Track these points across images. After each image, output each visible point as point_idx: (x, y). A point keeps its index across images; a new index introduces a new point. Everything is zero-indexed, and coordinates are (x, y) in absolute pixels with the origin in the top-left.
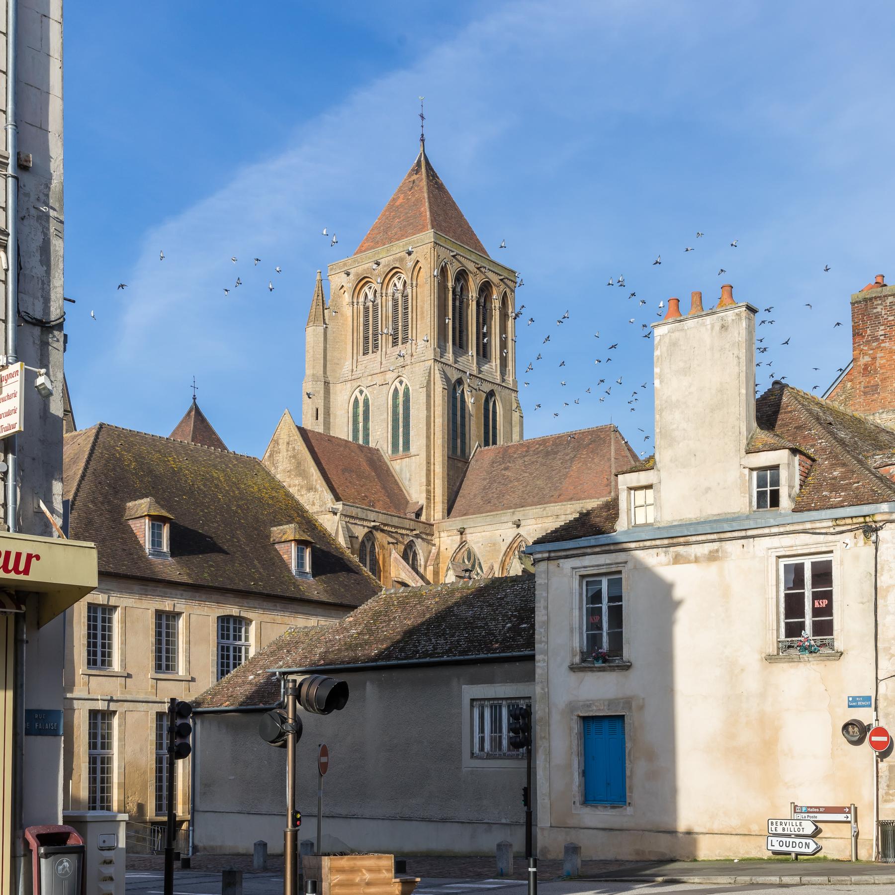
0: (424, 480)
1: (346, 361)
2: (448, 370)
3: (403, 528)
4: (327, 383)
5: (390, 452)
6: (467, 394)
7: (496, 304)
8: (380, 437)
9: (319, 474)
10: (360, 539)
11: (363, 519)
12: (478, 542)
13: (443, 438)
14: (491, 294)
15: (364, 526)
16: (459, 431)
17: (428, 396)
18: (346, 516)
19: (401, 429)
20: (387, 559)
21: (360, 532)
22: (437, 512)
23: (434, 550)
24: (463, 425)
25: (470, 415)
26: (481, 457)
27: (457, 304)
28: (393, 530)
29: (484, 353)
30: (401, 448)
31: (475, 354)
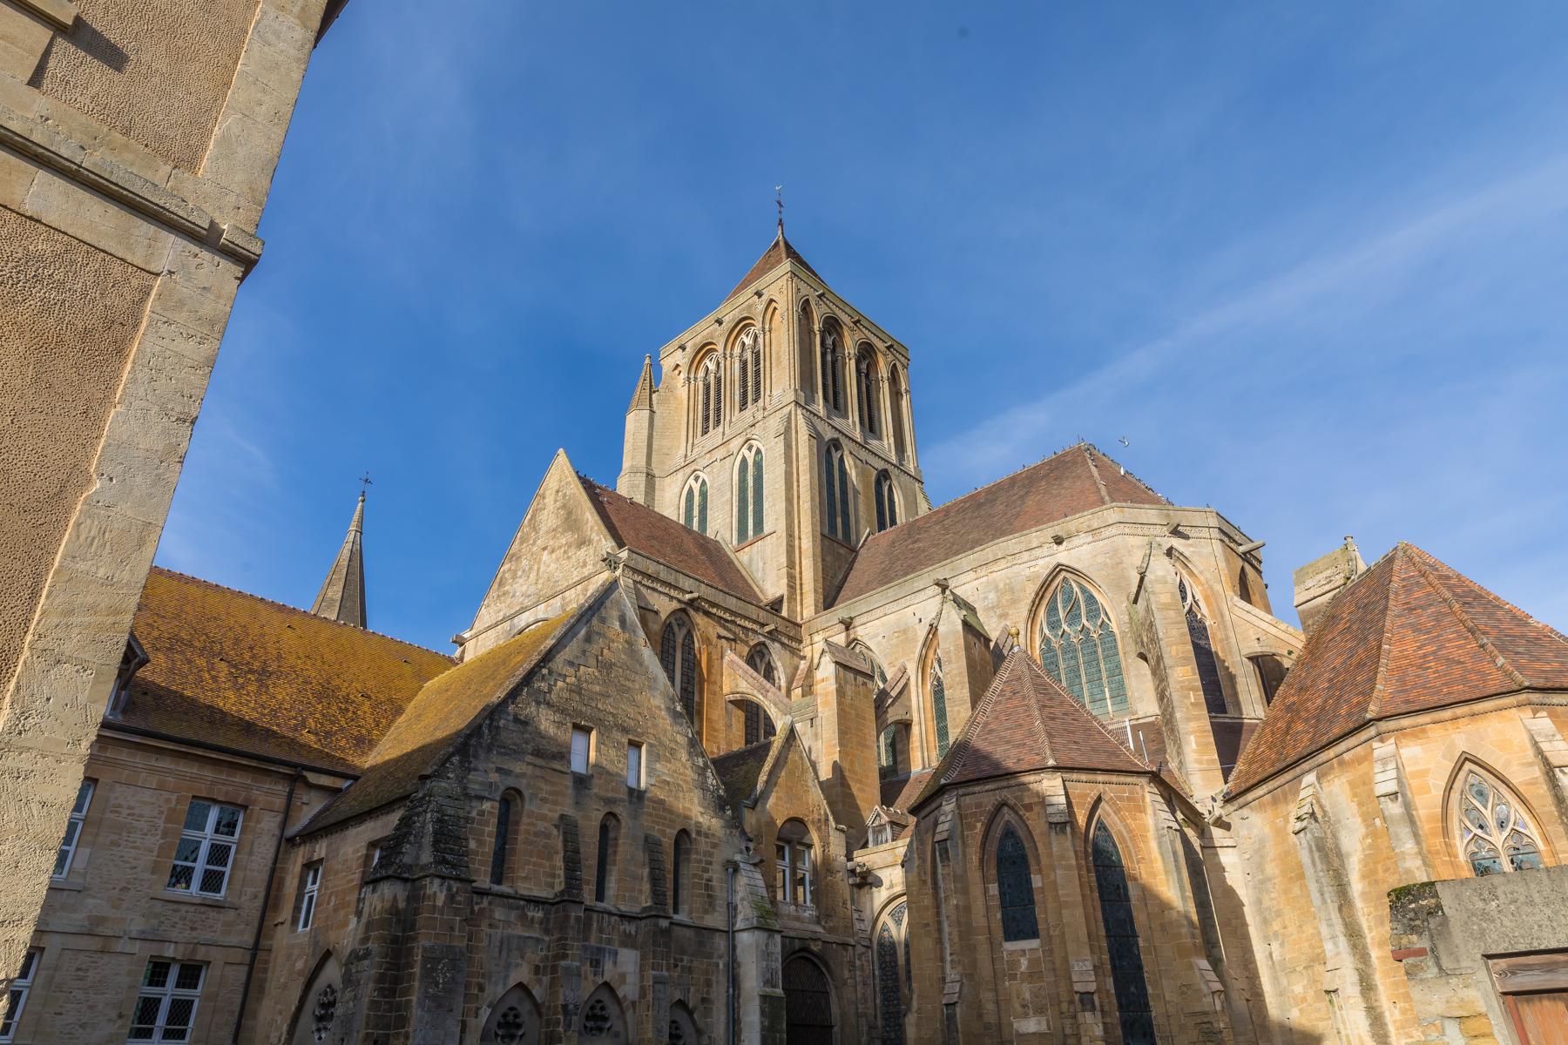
0: (783, 560)
1: (675, 445)
2: (820, 426)
3: (746, 618)
4: (650, 477)
5: (735, 542)
6: (849, 463)
7: (883, 371)
8: (721, 525)
9: (597, 518)
10: (663, 616)
11: (670, 585)
12: (876, 636)
13: (812, 499)
14: (876, 363)
15: (672, 598)
16: (839, 507)
17: (788, 446)
18: (635, 571)
19: (750, 508)
20: (716, 663)
21: (664, 605)
22: (807, 608)
23: (803, 665)
24: (845, 502)
25: (856, 492)
26: (872, 543)
27: (829, 358)
28: (727, 616)
29: (871, 425)
30: (751, 533)
31: (857, 419)
